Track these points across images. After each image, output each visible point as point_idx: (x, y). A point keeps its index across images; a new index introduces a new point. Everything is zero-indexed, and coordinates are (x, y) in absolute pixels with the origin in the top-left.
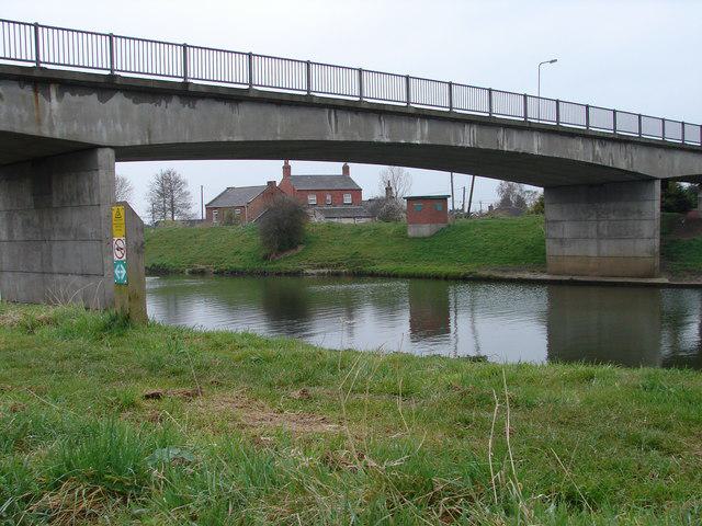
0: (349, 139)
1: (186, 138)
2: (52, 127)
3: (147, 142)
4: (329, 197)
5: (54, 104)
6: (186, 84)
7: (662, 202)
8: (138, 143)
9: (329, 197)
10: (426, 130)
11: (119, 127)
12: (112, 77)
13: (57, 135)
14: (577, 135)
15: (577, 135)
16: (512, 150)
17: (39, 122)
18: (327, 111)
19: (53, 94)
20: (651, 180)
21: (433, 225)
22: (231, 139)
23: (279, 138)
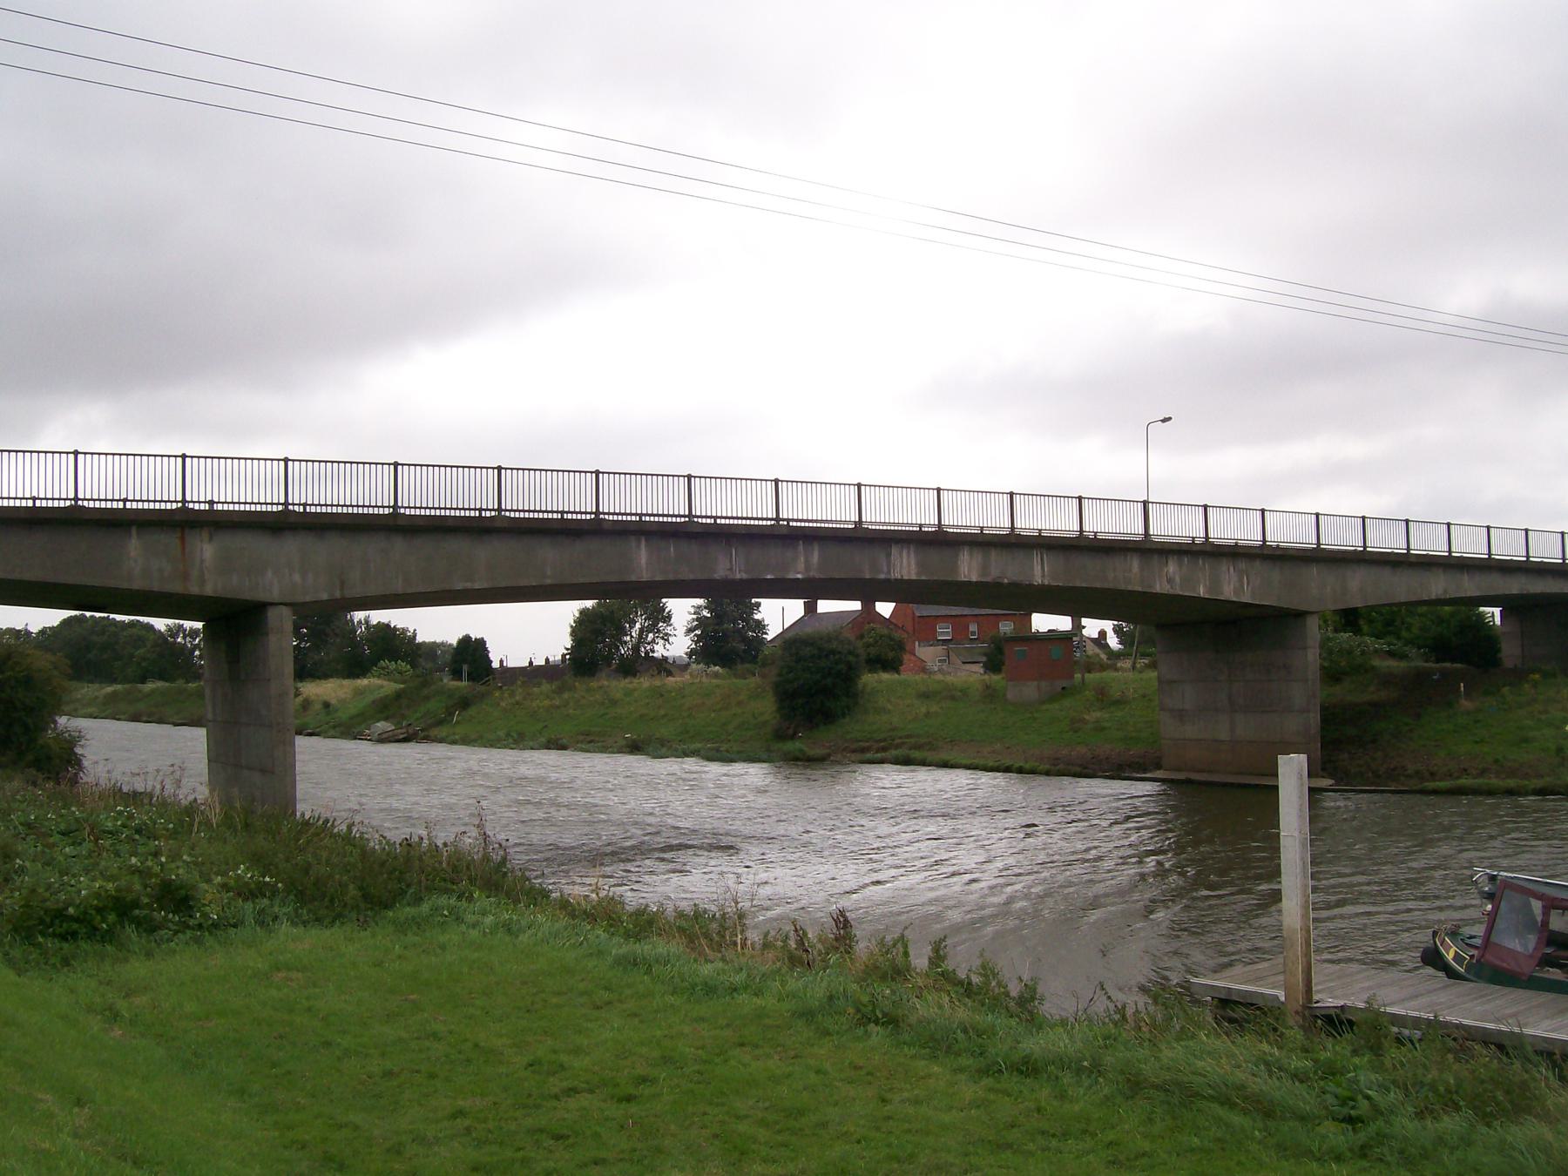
0: (671, 577)
1: (689, 576)
2: (202, 582)
3: (338, 594)
4: (973, 627)
5: (206, 550)
6: (395, 515)
7: (1412, 605)
8: (325, 596)
9: (973, 627)
10: (815, 557)
11: (297, 577)
12: (286, 513)
13: (209, 590)
14: (1129, 550)
15: (1129, 550)
16: (988, 579)
17: (186, 577)
18: (633, 538)
19: (801, 547)
20: (1300, 615)
21: (1043, 684)
22: (469, 585)
23: (549, 581)
